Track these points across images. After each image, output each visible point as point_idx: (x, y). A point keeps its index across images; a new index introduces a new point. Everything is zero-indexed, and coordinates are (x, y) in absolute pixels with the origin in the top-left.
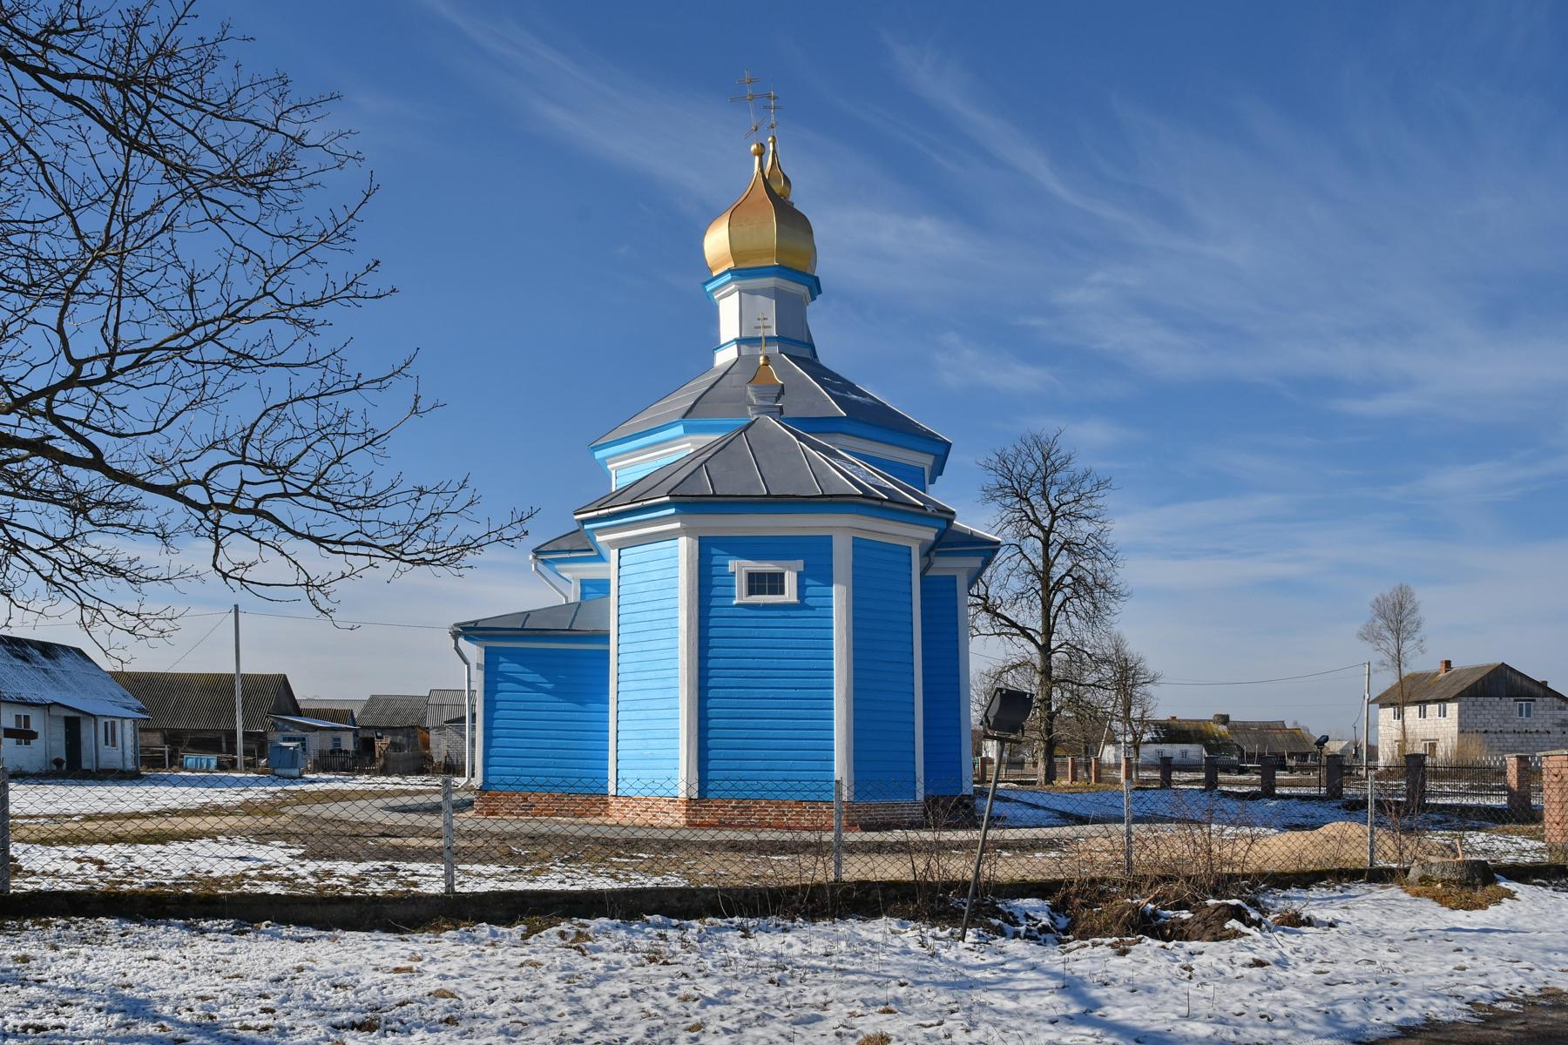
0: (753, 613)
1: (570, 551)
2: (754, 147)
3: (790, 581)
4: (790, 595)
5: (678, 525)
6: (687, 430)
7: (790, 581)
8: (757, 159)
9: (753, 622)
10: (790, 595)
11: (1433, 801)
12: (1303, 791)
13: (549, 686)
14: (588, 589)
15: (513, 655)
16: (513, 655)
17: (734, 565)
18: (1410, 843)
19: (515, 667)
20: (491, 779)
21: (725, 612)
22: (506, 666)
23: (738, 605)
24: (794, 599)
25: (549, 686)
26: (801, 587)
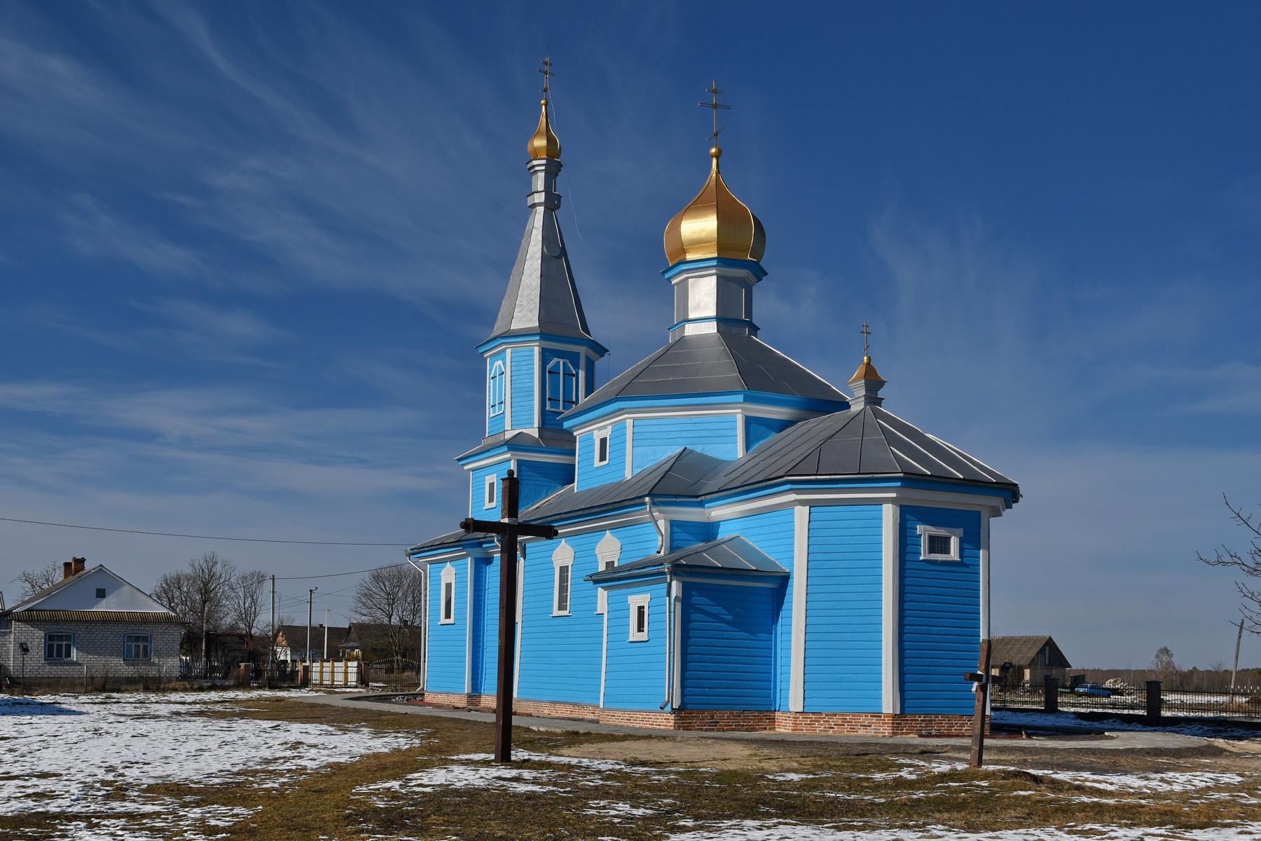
0: (932, 567)
1: (676, 496)
2: (713, 150)
3: (954, 543)
4: (954, 554)
5: (894, 495)
6: (746, 400)
7: (954, 543)
8: (714, 161)
9: (931, 574)
10: (954, 554)
11: (1065, 709)
12: (1034, 707)
13: (729, 617)
14: (675, 529)
15: (702, 589)
16: (702, 589)
17: (920, 529)
18: (395, 745)
19: (704, 600)
20: (687, 699)
21: (915, 566)
22: (697, 599)
23: (923, 561)
24: (957, 559)
25: (729, 617)
26: (961, 549)
